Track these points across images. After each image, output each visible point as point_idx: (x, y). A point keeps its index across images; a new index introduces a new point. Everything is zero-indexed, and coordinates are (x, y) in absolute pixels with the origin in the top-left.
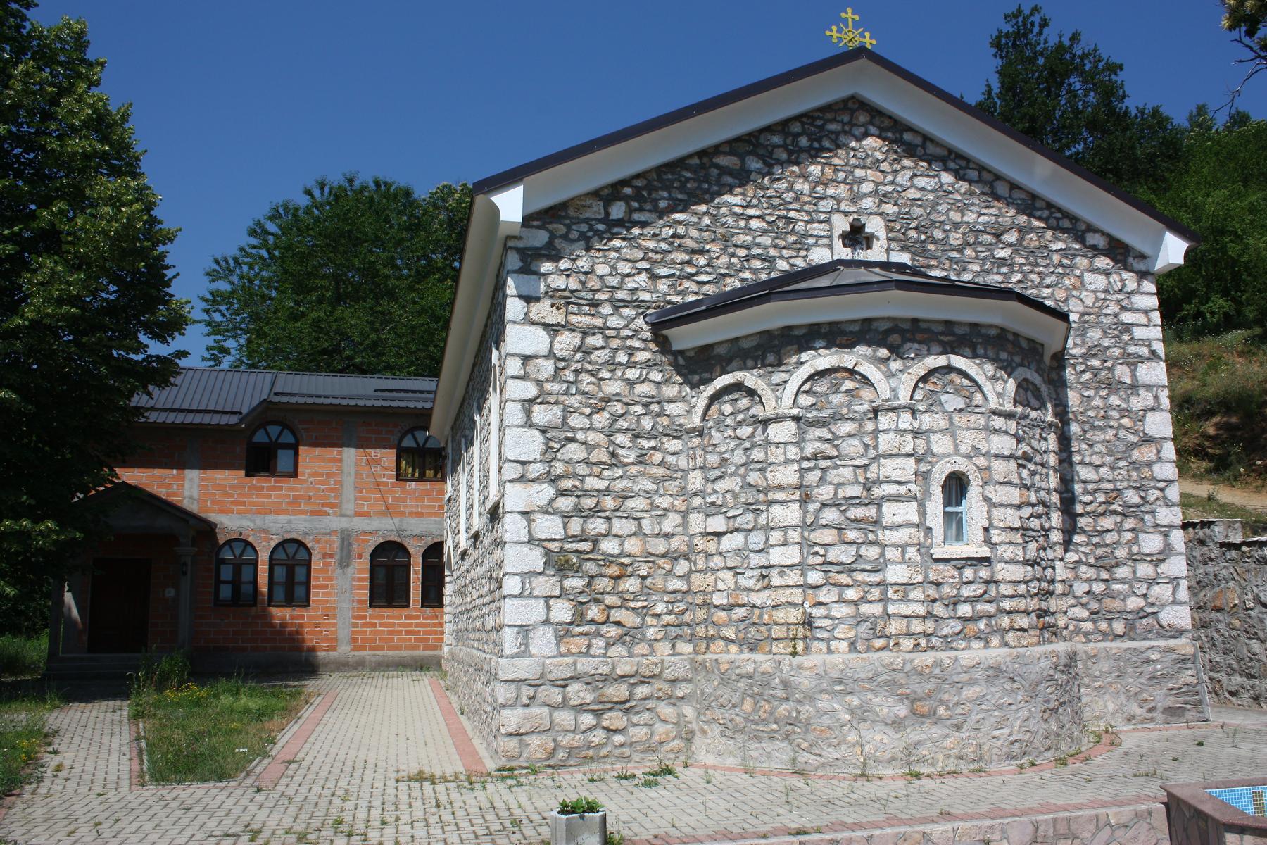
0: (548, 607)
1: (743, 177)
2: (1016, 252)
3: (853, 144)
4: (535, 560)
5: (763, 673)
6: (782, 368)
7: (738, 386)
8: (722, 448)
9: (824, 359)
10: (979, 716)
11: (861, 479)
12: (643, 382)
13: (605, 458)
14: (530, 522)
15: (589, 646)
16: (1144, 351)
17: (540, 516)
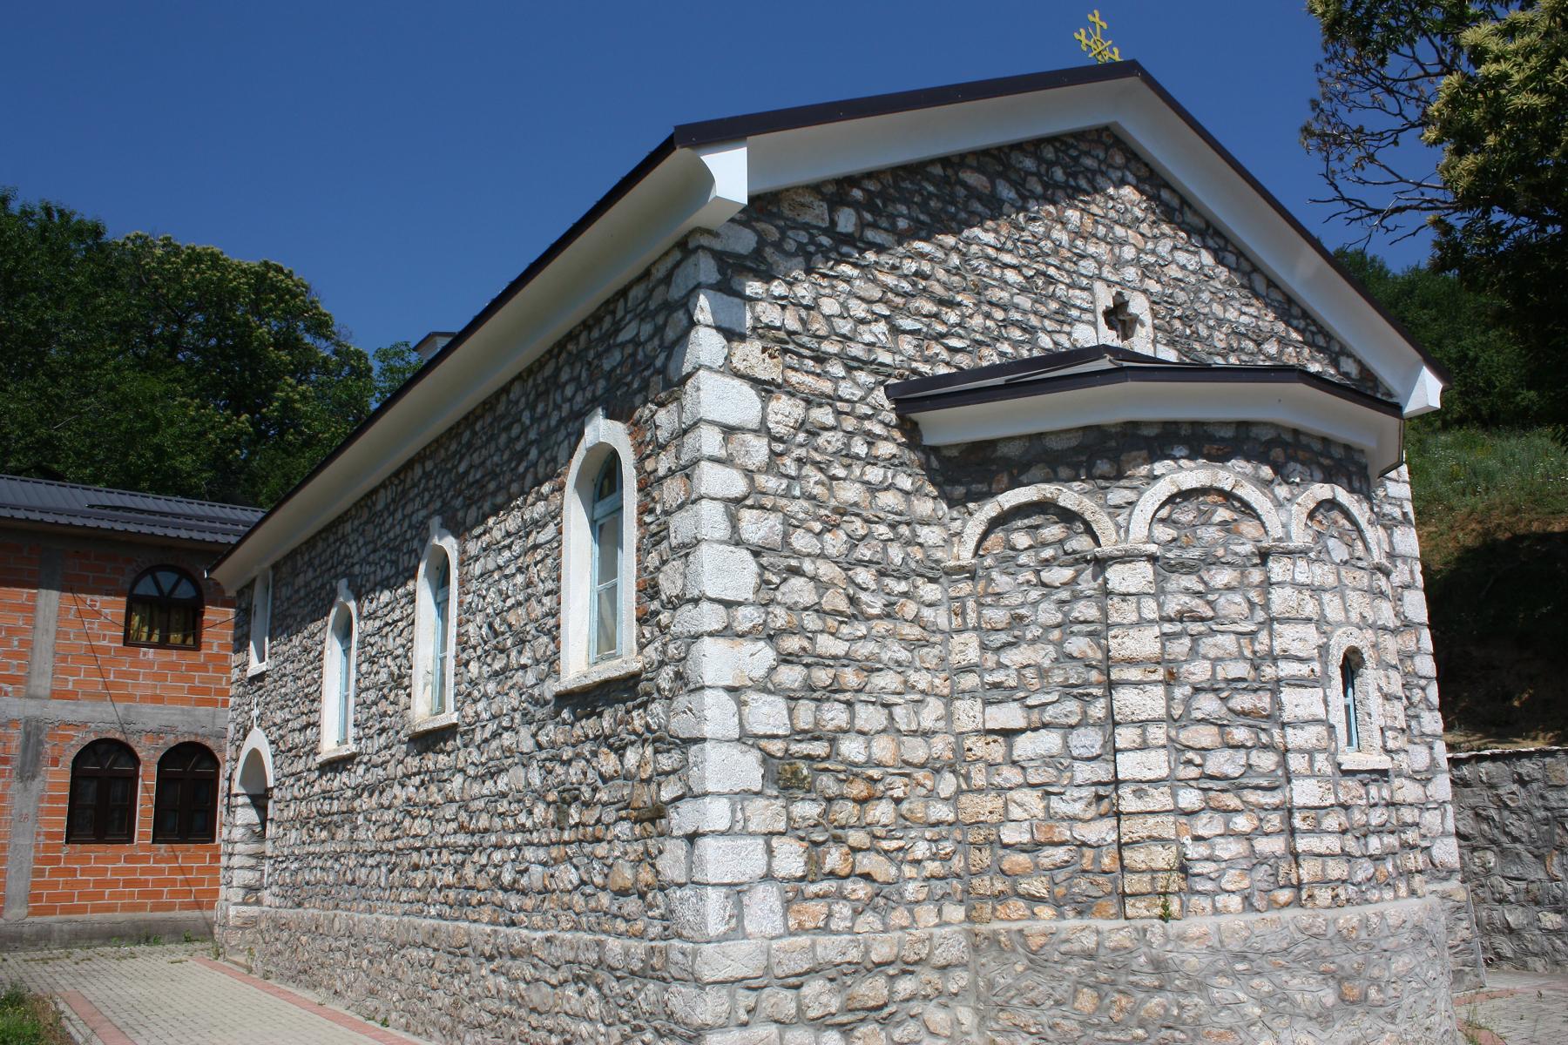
0: (770, 851)
1: (994, 209)
3: (1111, 191)
4: (748, 770)
5: (1114, 950)
6: (1122, 483)
7: (1042, 507)
8: (1017, 599)
9: (1193, 474)
11: (1247, 653)
12: (887, 489)
13: (843, 605)
14: (741, 704)
15: (829, 916)
16: (1397, 513)
17: (755, 695)
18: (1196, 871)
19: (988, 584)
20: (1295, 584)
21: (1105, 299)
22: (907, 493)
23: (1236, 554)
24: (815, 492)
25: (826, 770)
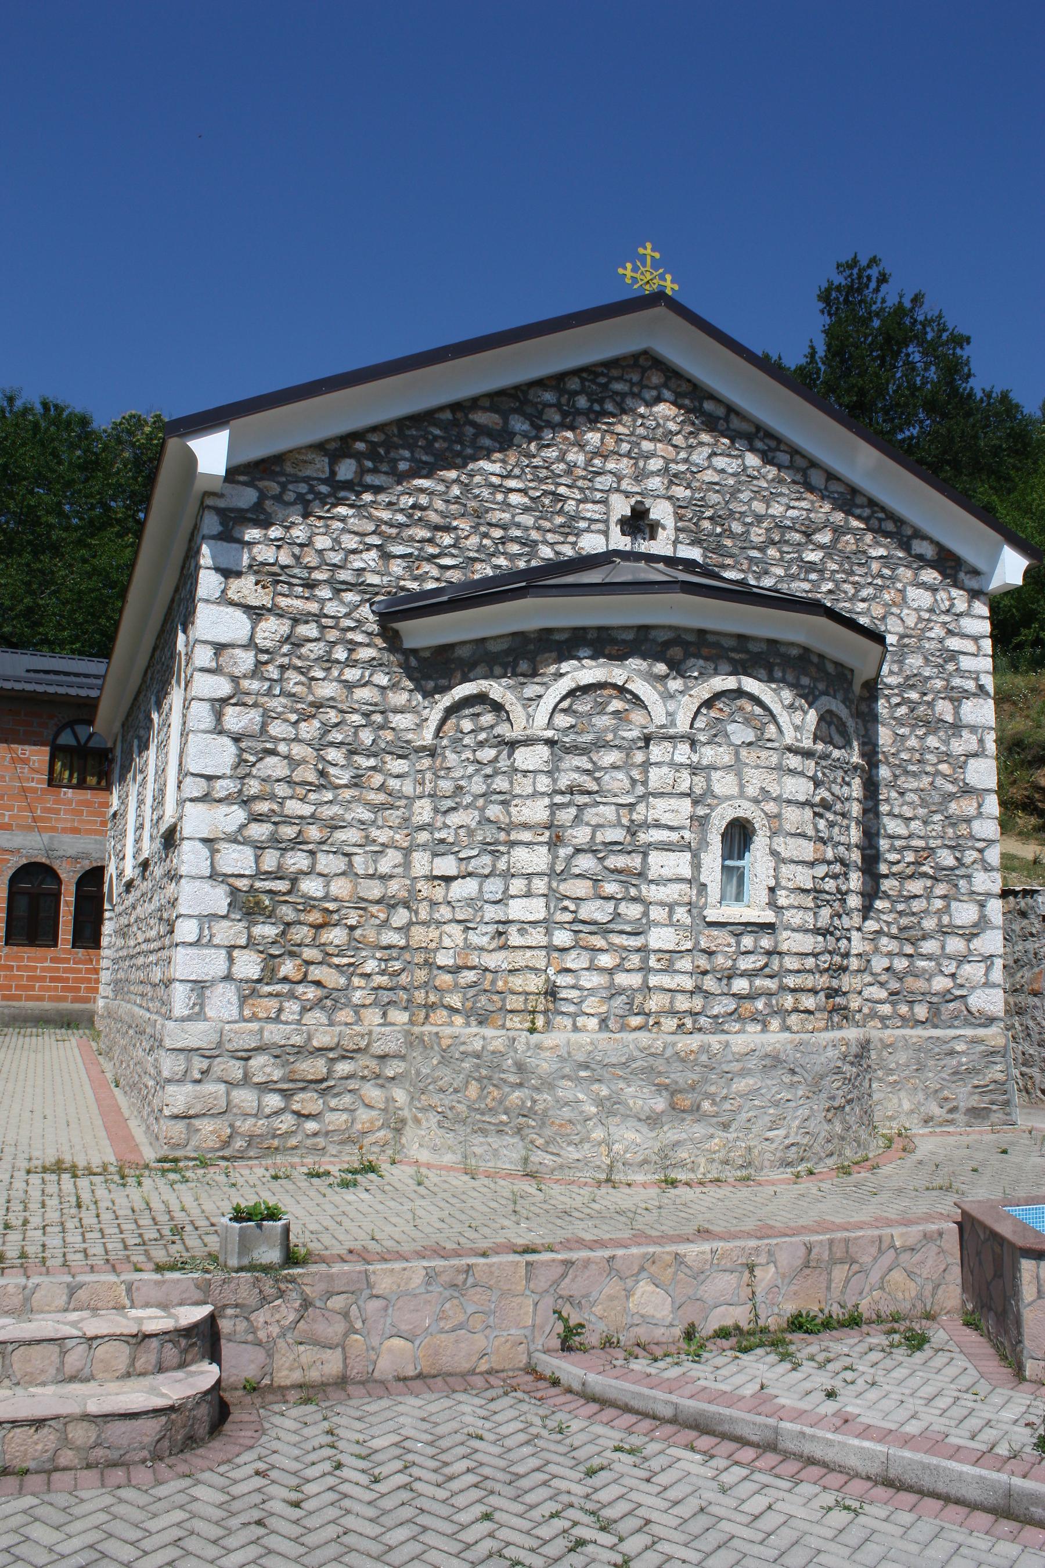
0: (231, 960)
1: (504, 440)
2: (829, 555)
3: (642, 410)
4: (218, 899)
5: (493, 1052)
6: (536, 680)
7: (481, 698)
8: (457, 774)
9: (588, 671)
12: (364, 685)
13: (312, 777)
14: (214, 852)
15: (280, 1010)
16: (970, 685)
18: (562, 996)
19: (443, 761)
20: (672, 764)
21: (621, 507)
22: (384, 688)
23: (624, 738)
24: (294, 691)
25: (286, 902)
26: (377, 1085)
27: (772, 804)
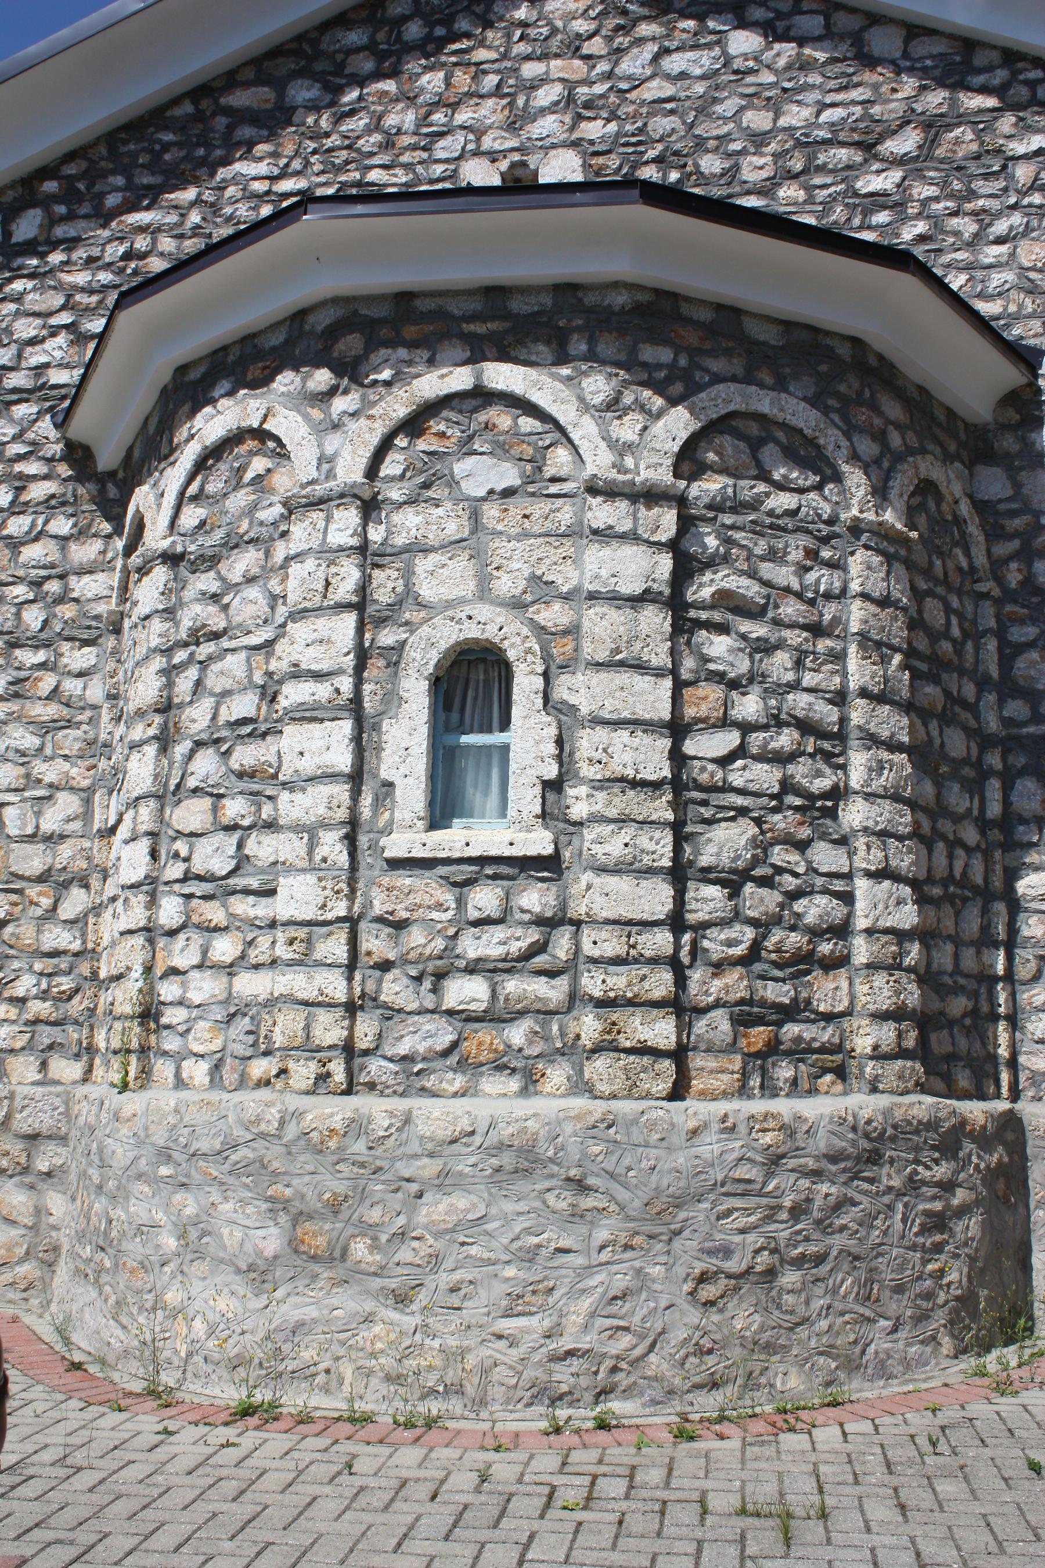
1: (274, 120)
2: (919, 174)
10: (457, 1276)
12: (36, 539)
26: (23, 1185)
27: (557, 606)
